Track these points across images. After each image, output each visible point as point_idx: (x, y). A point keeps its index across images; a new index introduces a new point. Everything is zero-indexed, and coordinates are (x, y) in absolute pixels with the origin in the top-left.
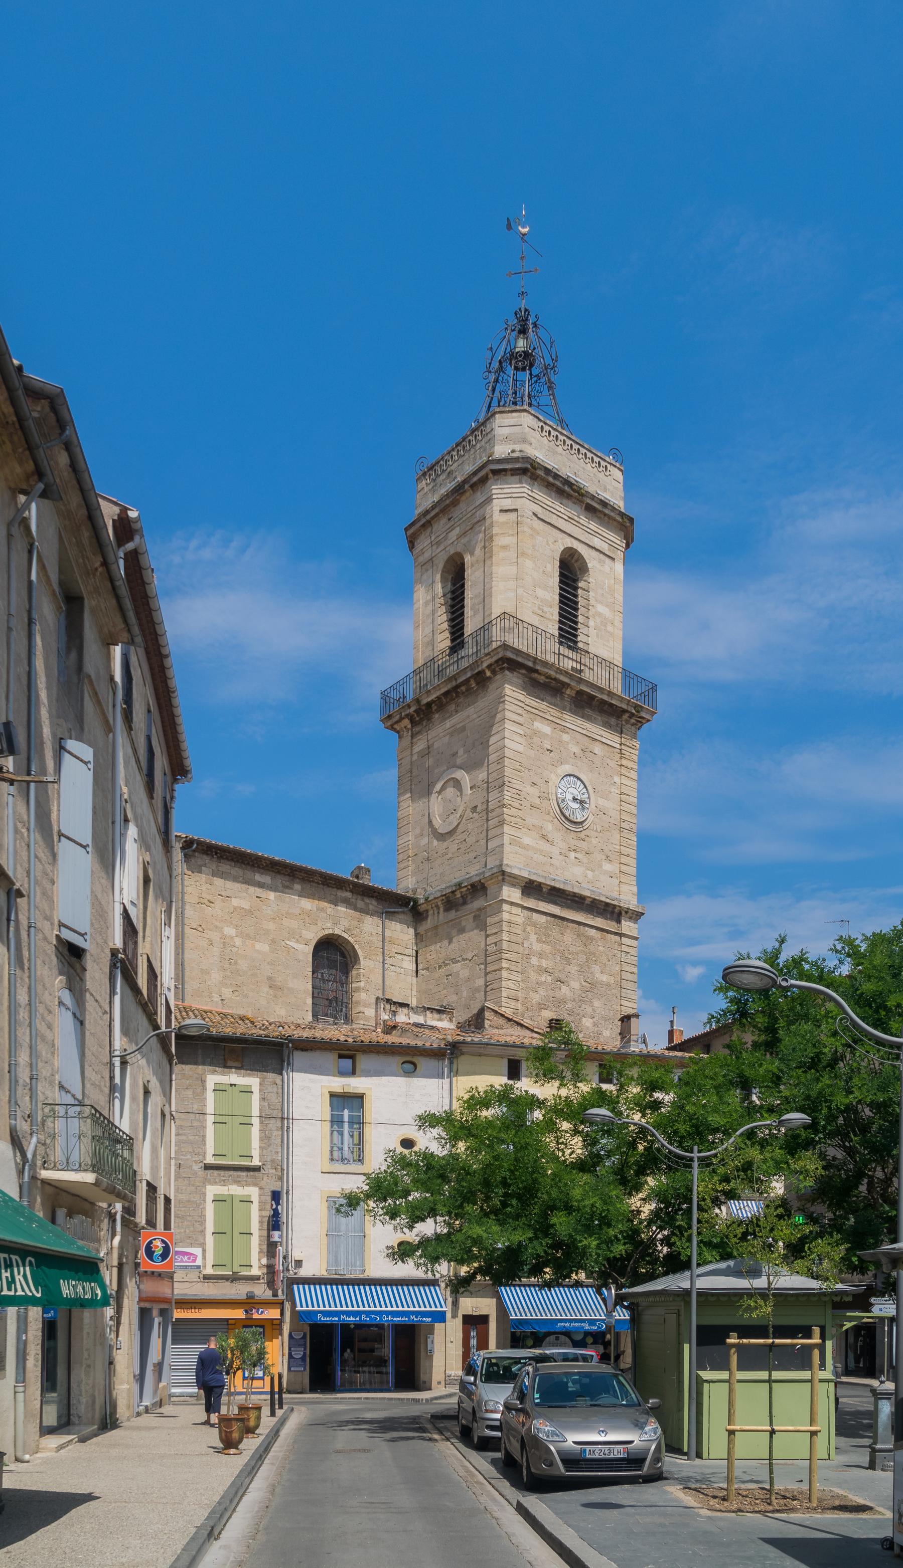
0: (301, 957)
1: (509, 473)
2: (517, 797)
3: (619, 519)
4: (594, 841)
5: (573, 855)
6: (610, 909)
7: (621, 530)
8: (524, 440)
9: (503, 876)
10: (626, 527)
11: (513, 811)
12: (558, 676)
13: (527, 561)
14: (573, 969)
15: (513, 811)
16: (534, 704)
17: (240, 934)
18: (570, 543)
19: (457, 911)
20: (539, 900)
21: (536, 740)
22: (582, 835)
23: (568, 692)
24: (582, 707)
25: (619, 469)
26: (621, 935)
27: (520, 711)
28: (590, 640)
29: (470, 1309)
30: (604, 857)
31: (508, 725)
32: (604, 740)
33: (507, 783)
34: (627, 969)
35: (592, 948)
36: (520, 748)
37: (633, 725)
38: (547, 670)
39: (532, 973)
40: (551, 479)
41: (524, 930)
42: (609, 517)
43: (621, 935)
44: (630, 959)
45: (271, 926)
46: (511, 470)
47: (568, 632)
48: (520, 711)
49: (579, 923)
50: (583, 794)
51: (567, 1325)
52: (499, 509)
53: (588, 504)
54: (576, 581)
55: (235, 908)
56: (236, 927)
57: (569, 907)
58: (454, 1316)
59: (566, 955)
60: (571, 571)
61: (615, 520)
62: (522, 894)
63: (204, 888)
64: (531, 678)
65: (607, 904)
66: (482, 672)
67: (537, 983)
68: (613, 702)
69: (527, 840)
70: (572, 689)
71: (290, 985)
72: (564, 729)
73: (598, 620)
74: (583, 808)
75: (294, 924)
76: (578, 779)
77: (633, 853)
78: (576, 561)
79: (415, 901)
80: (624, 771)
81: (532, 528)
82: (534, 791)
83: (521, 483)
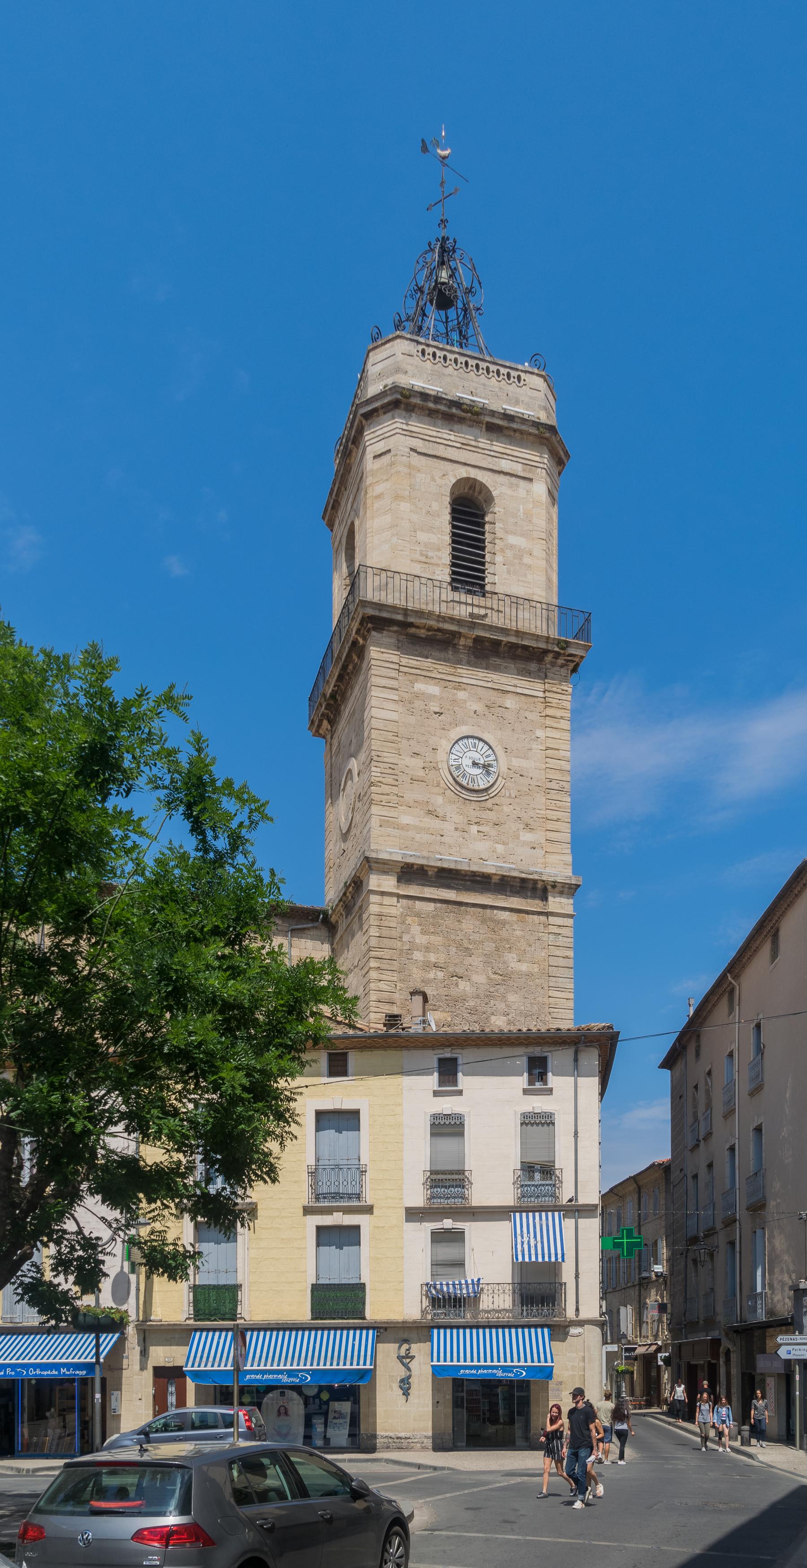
1: (381, 412)
2: (391, 771)
3: (533, 431)
4: (507, 809)
5: (474, 829)
6: (530, 886)
7: (542, 444)
8: (398, 370)
9: (370, 864)
10: (547, 439)
11: (385, 789)
12: (441, 625)
13: (402, 504)
14: (476, 961)
15: (385, 789)
16: (413, 663)
18: (463, 472)
20: (423, 885)
22: (489, 804)
23: (462, 641)
24: (485, 657)
25: (537, 375)
26: (547, 914)
28: (497, 579)
29: (162, 1360)
31: (375, 692)
32: (519, 690)
33: (375, 758)
34: (557, 953)
35: (504, 933)
36: (394, 716)
37: (562, 666)
38: (424, 621)
39: (415, 970)
40: (431, 405)
41: (403, 922)
42: (521, 432)
43: (547, 914)
44: (561, 941)
46: (382, 407)
49: (484, 907)
50: (488, 756)
51: (259, 1377)
52: (372, 455)
53: (487, 423)
54: (483, 516)
57: (468, 889)
58: (143, 1368)
60: (469, 511)
61: (530, 434)
62: (398, 882)
64: (407, 635)
65: (523, 880)
67: (423, 981)
68: (525, 643)
69: (405, 820)
70: (466, 638)
72: (459, 686)
74: (488, 773)
76: (480, 739)
77: (567, 817)
78: (480, 493)
79: (325, 913)
80: (549, 722)
81: (409, 466)
82: (417, 762)
83: (393, 418)
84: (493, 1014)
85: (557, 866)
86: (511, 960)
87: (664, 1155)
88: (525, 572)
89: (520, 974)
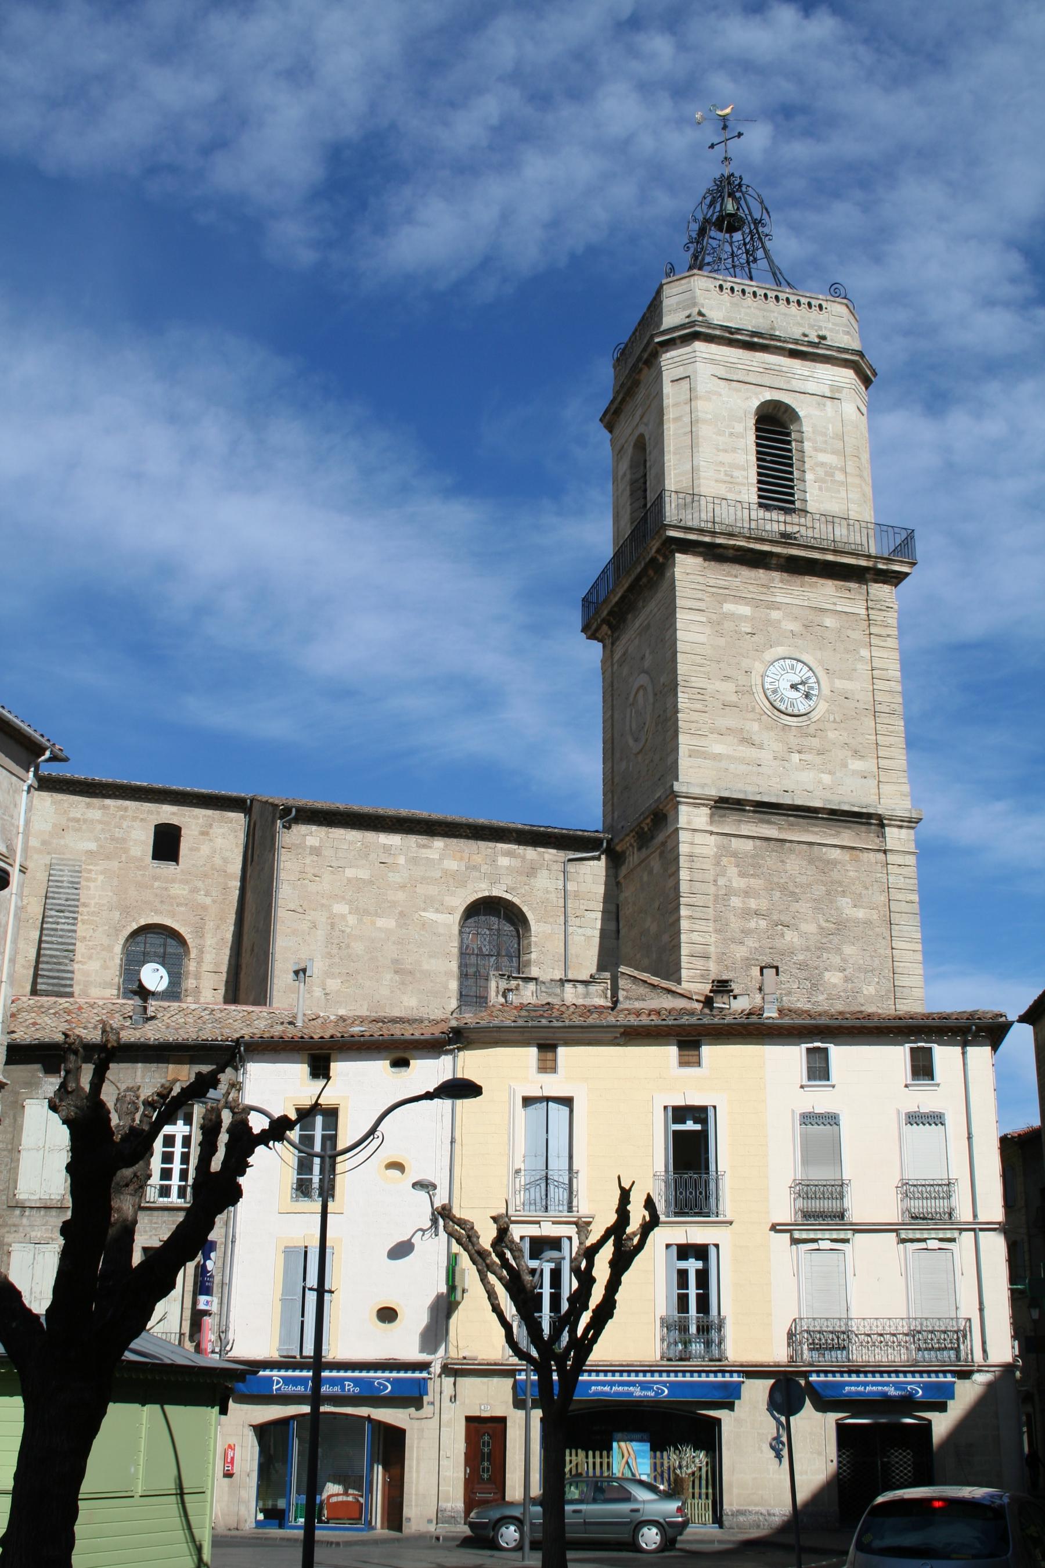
0: (441, 930)
2: (700, 697)
4: (831, 735)
5: (796, 757)
14: (804, 907)
17: (355, 910)
18: (768, 395)
19: (647, 848)
21: (728, 625)
27: (699, 595)
30: (850, 753)
34: (900, 897)
35: (835, 875)
39: (733, 919)
41: (718, 864)
45: (401, 896)
48: (699, 595)
55: (349, 880)
56: (350, 902)
59: (791, 889)
60: (775, 425)
63: (308, 861)
66: (653, 560)
69: (718, 748)
71: (426, 966)
72: (774, 606)
73: (821, 472)
75: (432, 890)
80: (875, 641)
82: (729, 687)
85: (893, 798)
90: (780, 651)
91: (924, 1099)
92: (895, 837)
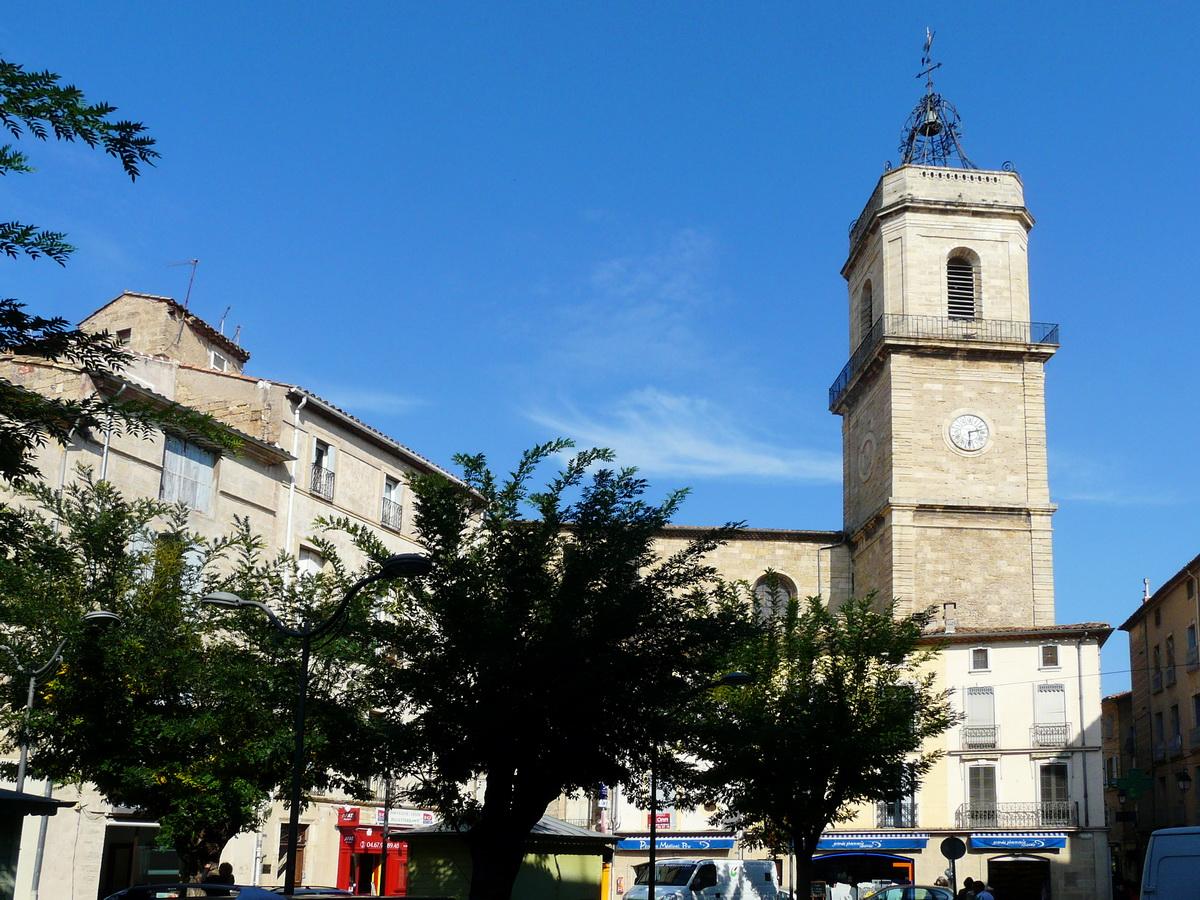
4: (996, 461)
14: (974, 567)
18: (957, 244)
32: (1003, 380)
36: (908, 407)
47: (322, 448)
60: (961, 265)
66: (876, 360)
69: (919, 475)
72: (957, 383)
73: (992, 291)
82: (927, 436)
84: (989, 604)
85: (1039, 497)
86: (1004, 566)
87: (1128, 688)
88: (1006, 303)
89: (1010, 575)
90: (962, 411)
91: (1051, 676)
92: (1037, 521)
